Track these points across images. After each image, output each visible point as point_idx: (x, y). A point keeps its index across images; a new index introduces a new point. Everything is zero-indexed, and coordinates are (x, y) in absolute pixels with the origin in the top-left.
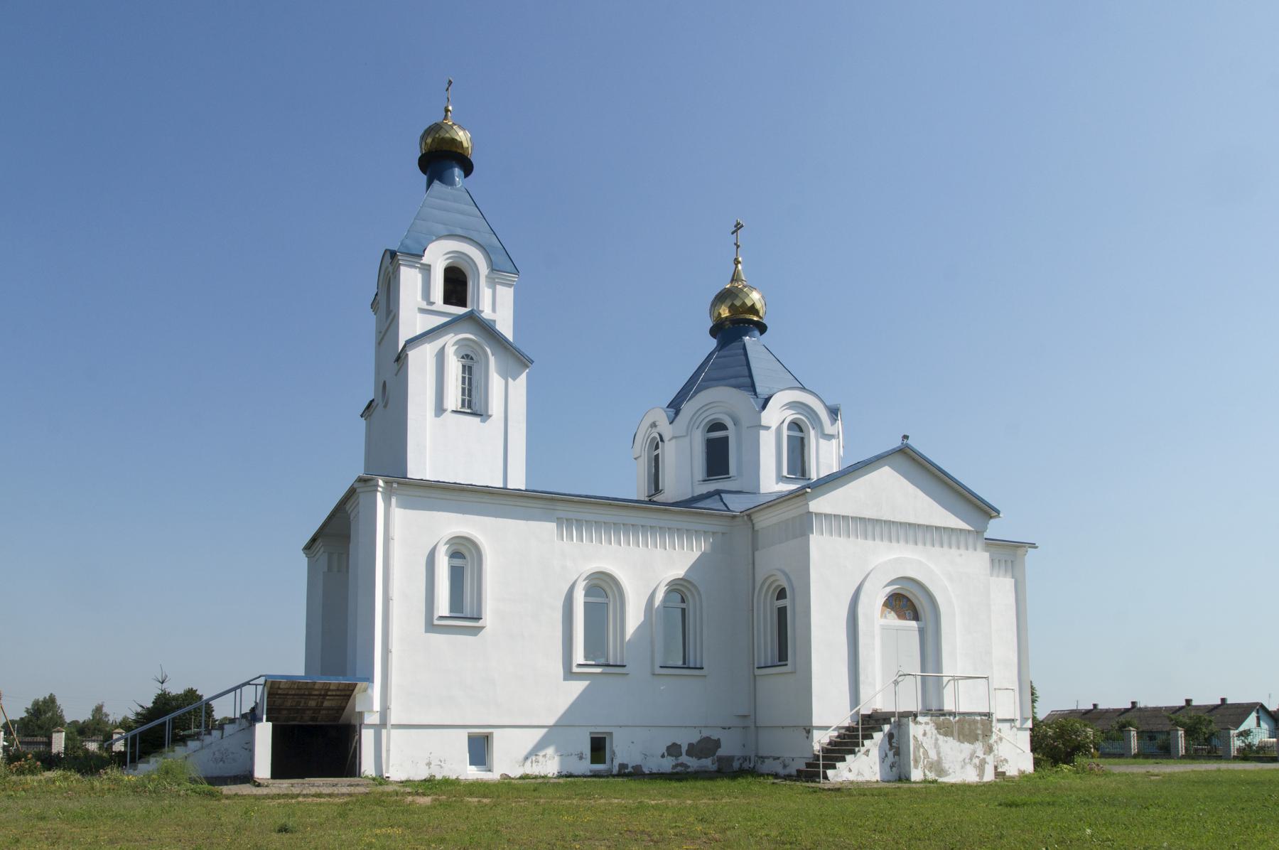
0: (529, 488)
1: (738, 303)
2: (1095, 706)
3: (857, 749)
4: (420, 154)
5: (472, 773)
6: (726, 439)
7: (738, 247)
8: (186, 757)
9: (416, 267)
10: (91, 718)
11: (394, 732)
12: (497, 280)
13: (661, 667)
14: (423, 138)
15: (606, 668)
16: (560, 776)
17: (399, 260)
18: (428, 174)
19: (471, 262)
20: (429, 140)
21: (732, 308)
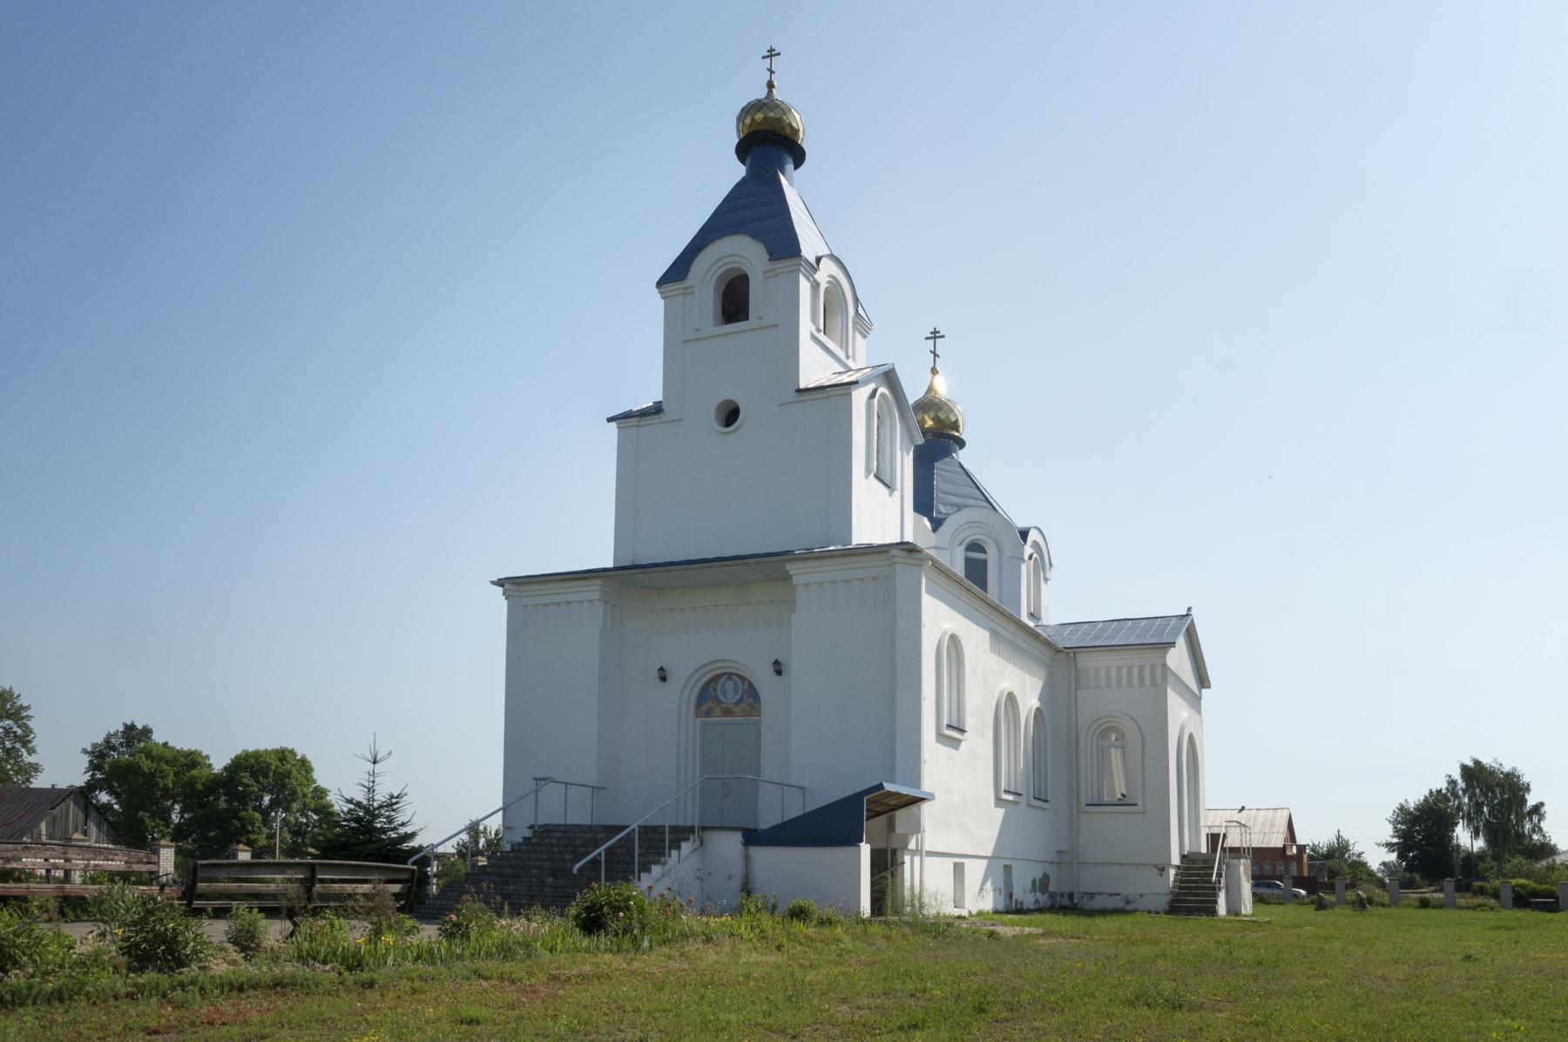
0: (616, 565)
1: (942, 415)
2: (53, 786)
3: (663, 859)
4: (737, 140)
5: (957, 912)
6: (985, 562)
7: (936, 355)
8: (730, 879)
9: (809, 280)
10: (39, 782)
11: (927, 860)
12: (858, 327)
13: (1087, 805)
14: (740, 118)
15: (1017, 796)
16: (996, 912)
17: (800, 270)
18: (748, 161)
19: (842, 297)
20: (748, 121)
21: (936, 419)
